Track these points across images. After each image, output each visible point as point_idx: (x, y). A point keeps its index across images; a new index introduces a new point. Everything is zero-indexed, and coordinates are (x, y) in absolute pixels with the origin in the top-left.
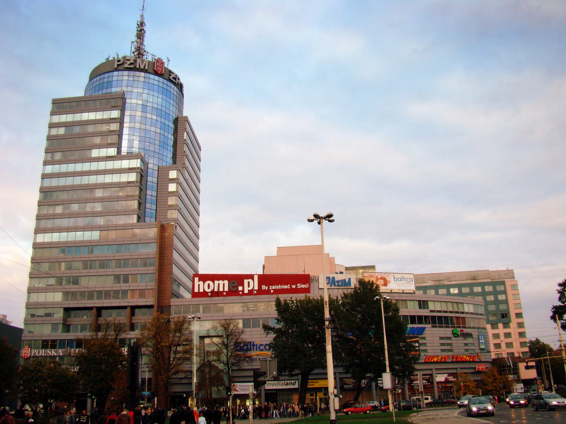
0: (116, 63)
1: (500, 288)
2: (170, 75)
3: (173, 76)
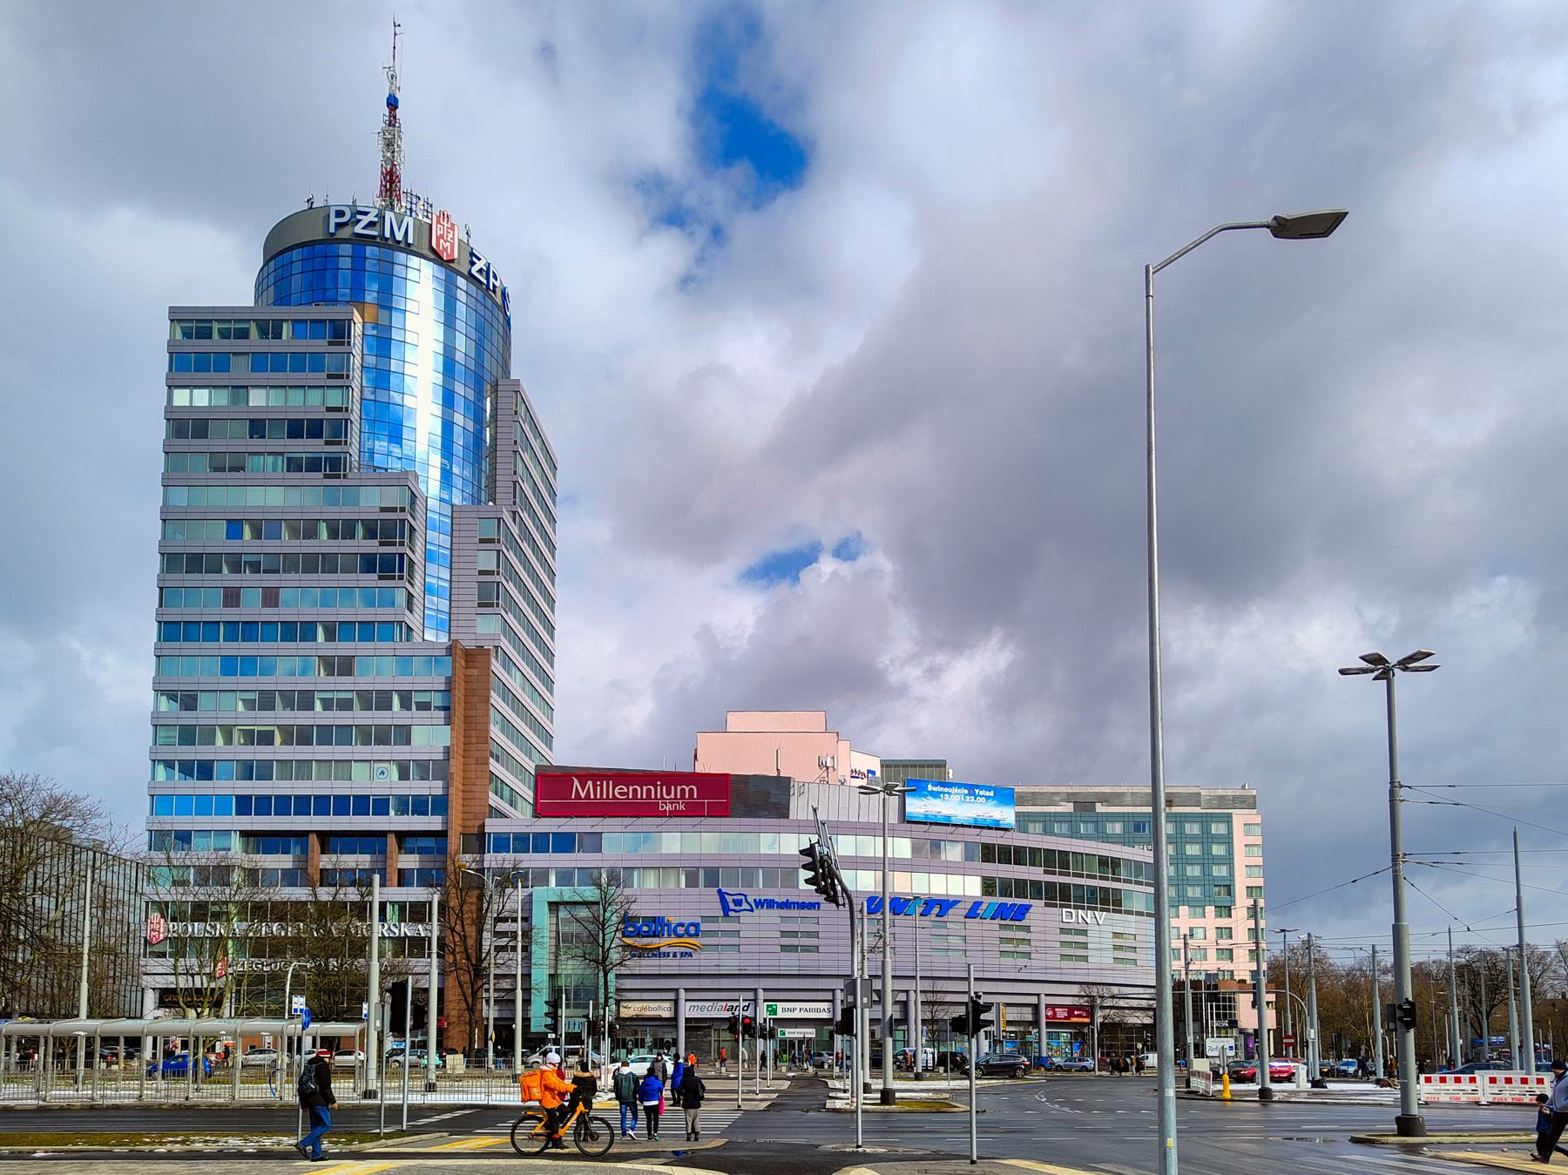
0: (333, 220)
1: (1218, 829)
2: (473, 263)
3: (479, 265)
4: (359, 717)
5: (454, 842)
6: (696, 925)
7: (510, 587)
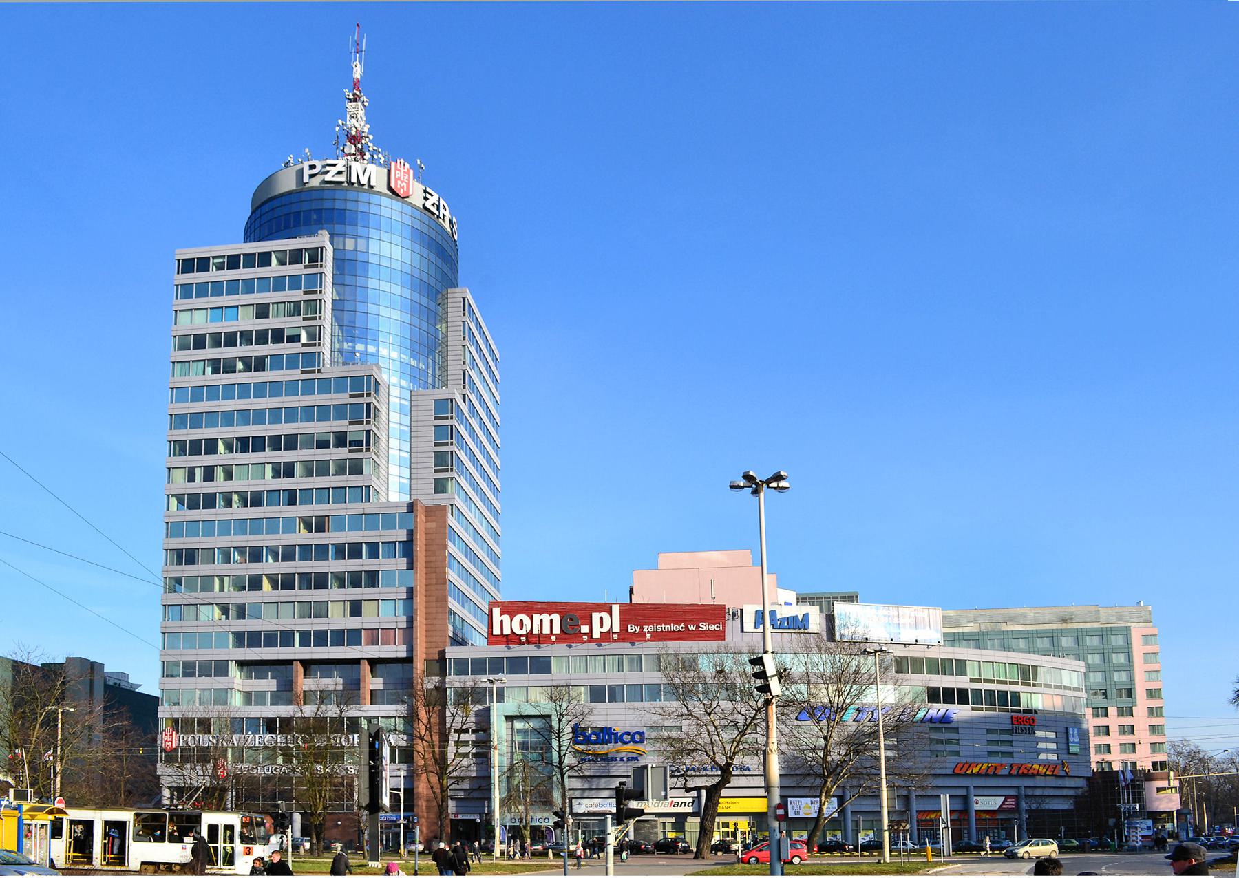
2: (426, 199)
4: (332, 565)
5: (420, 665)
6: (641, 734)
7: (462, 455)
